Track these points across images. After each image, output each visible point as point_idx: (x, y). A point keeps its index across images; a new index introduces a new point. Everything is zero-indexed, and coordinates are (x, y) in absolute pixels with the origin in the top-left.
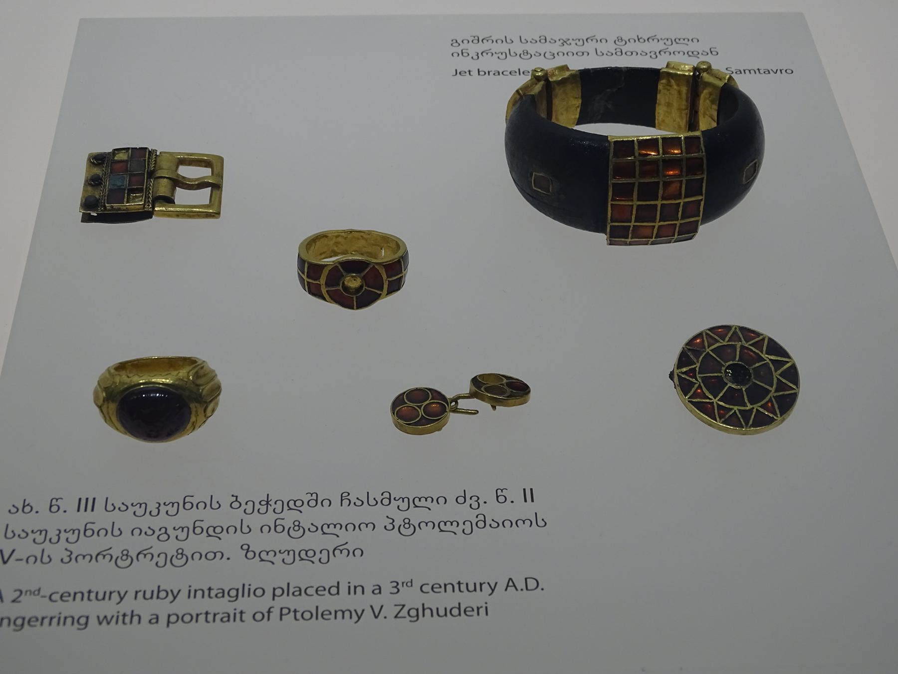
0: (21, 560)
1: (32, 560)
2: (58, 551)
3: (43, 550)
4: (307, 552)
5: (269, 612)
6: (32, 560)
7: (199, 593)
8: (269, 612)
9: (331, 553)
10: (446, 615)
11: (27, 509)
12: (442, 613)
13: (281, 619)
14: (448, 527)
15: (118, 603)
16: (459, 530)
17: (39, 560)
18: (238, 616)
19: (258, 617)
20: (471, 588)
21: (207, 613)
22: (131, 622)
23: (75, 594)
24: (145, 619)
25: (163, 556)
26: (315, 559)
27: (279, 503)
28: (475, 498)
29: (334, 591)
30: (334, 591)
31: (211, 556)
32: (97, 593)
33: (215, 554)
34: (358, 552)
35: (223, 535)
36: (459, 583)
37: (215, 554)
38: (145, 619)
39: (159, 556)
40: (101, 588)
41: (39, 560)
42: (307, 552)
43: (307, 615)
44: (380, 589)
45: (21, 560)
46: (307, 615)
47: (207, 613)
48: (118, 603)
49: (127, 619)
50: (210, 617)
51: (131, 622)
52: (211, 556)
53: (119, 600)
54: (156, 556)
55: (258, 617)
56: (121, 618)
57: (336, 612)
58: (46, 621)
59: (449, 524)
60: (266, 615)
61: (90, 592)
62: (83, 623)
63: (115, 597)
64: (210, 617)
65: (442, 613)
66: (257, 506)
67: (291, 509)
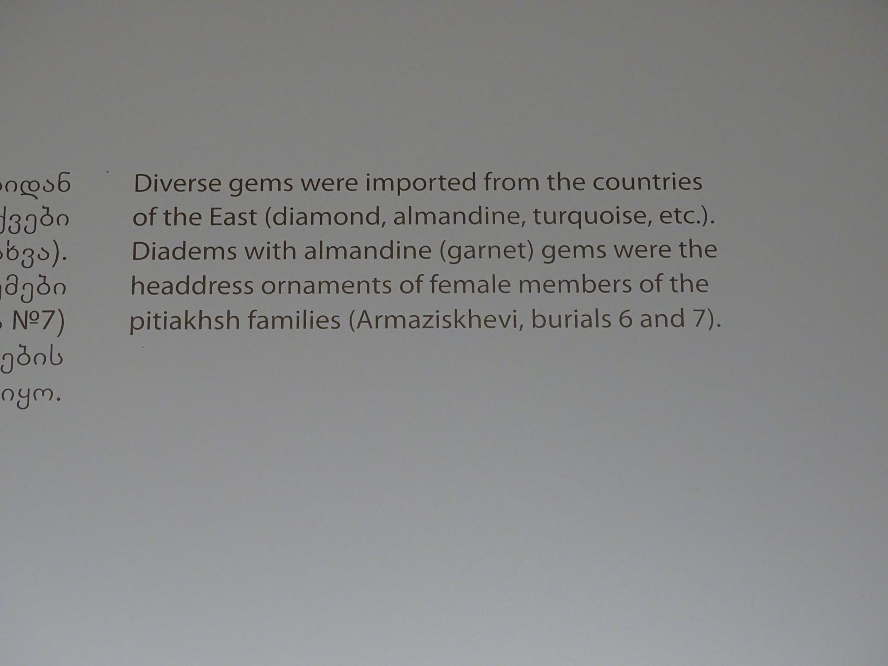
4: (30, 183)
5: (418, 281)
7: (644, 183)
8: (418, 281)
10: (595, 221)
12: (357, 217)
17: (48, 359)
18: (153, 321)
19: (140, 219)
20: (550, 218)
24: (301, 252)
25: (31, 218)
27: (31, 218)
28: (29, 253)
29: (469, 184)
30: (469, 184)
38: (301, 252)
41: (48, 359)
42: (30, 183)
43: (607, 217)
44: (661, 217)
46: (607, 217)
49: (280, 252)
50: (660, 183)
55: (140, 219)
56: (272, 251)
57: (456, 283)
58: (285, 287)
60: (149, 217)
62: (557, 181)
64: (660, 183)
65: (357, 217)
66: (23, 223)
67: (25, 194)
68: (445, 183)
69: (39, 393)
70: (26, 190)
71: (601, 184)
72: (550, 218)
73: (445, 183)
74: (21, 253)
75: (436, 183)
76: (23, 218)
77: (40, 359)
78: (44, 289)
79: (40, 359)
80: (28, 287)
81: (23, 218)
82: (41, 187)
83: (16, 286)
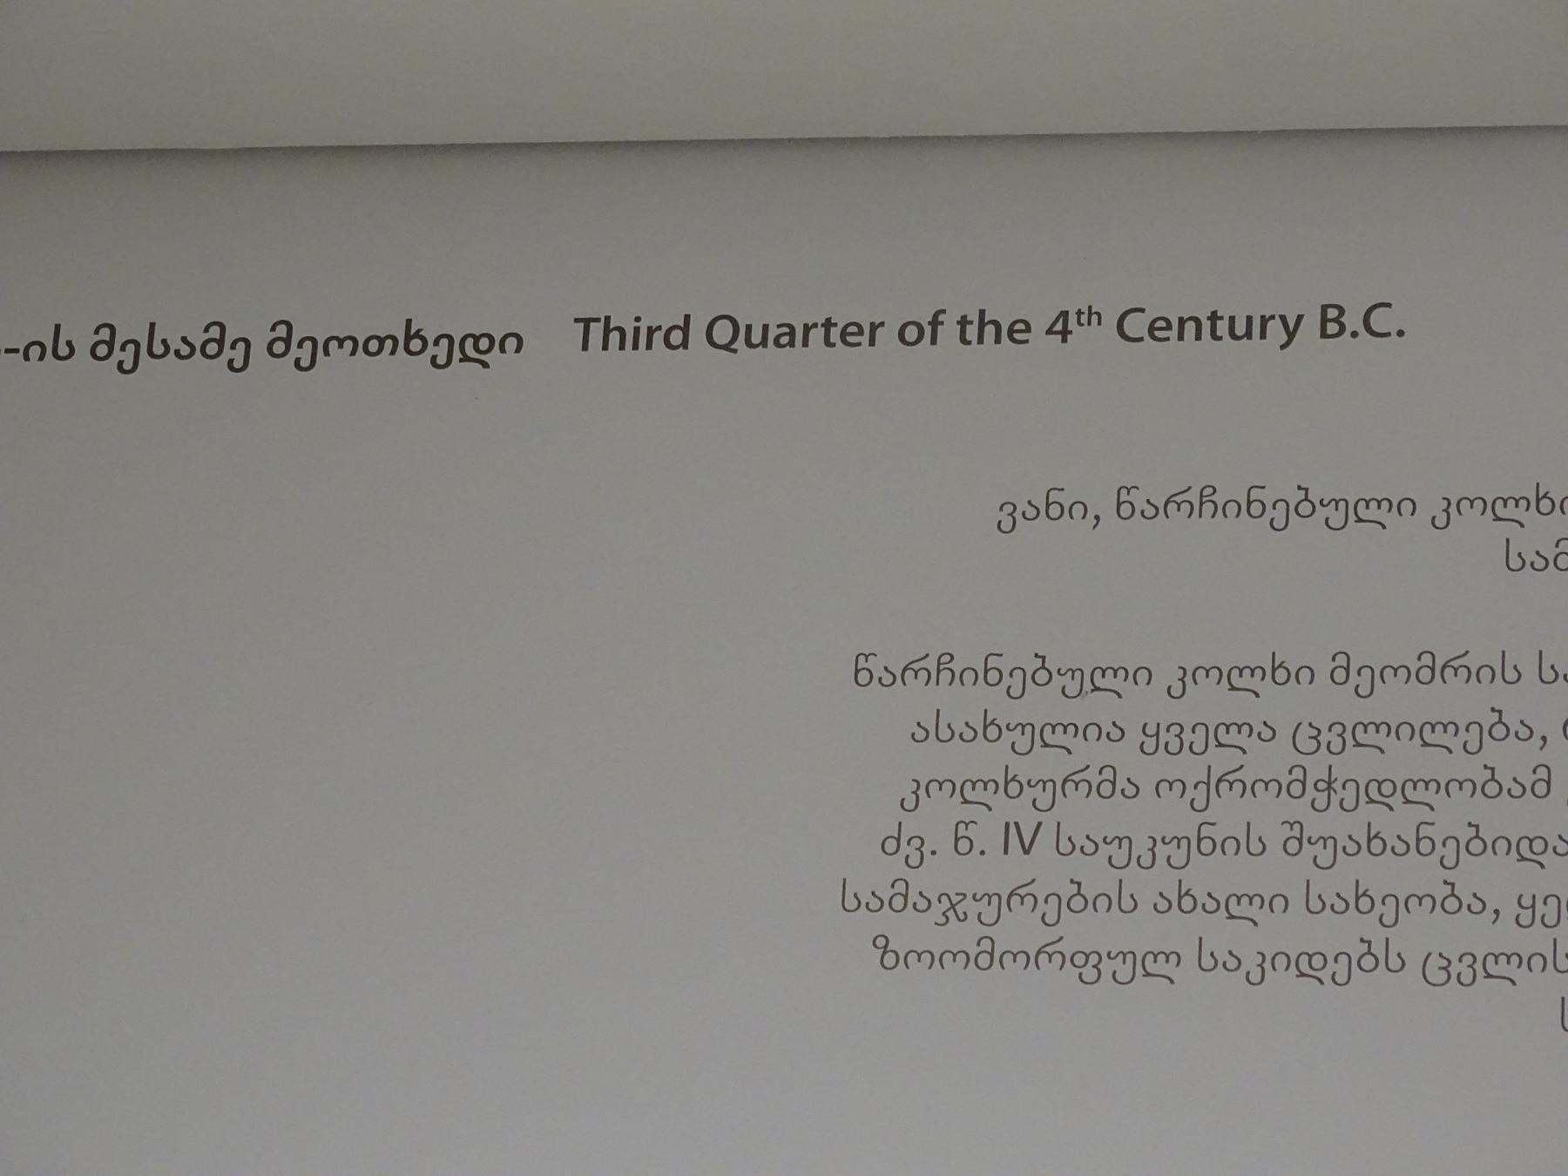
0: (17, 351)
1: (35, 351)
2: (1148, 884)
3: (1040, 824)
5: (935, 323)
6: (35, 351)
8: (935, 323)
9: (1402, 905)
11: (1365, 903)
13: (687, 318)
14: (1438, 737)
15: (1283, 347)
16: (1456, 744)
19: (911, 334)
20: (1240, 329)
21: (828, 324)
22: (981, 340)
23: (764, 342)
25: (1281, 505)
26: (1325, 975)
29: (676, 338)
31: (374, 346)
32: (1232, 319)
33: (1087, 957)
34: (511, 343)
35: (493, 357)
36: (1214, 317)
37: (1087, 957)
39: (436, 343)
40: (1238, 307)
42: (1380, 784)
45: (17, 351)
47: (828, 324)
48: (1283, 347)
49: (1084, 319)
51: (981, 340)
52: (374, 346)
53: (1285, 338)
54: (1041, 900)
55: (911, 334)
59: (1503, 959)
60: (928, 330)
61: (1214, 317)
63: (1276, 330)
66: (1187, 737)
68: (835, 334)
69: (1465, 504)
70: (1305, 968)
71: (1136, 325)
72: (1240, 329)
73: (835, 334)
74: (1378, 901)
75: (817, 335)
76: (1188, 729)
77: (1231, 846)
78: (1476, 846)
79: (1231, 846)
80: (1366, 672)
81: (1188, 729)
82: (1138, 512)
83: (1304, 784)
